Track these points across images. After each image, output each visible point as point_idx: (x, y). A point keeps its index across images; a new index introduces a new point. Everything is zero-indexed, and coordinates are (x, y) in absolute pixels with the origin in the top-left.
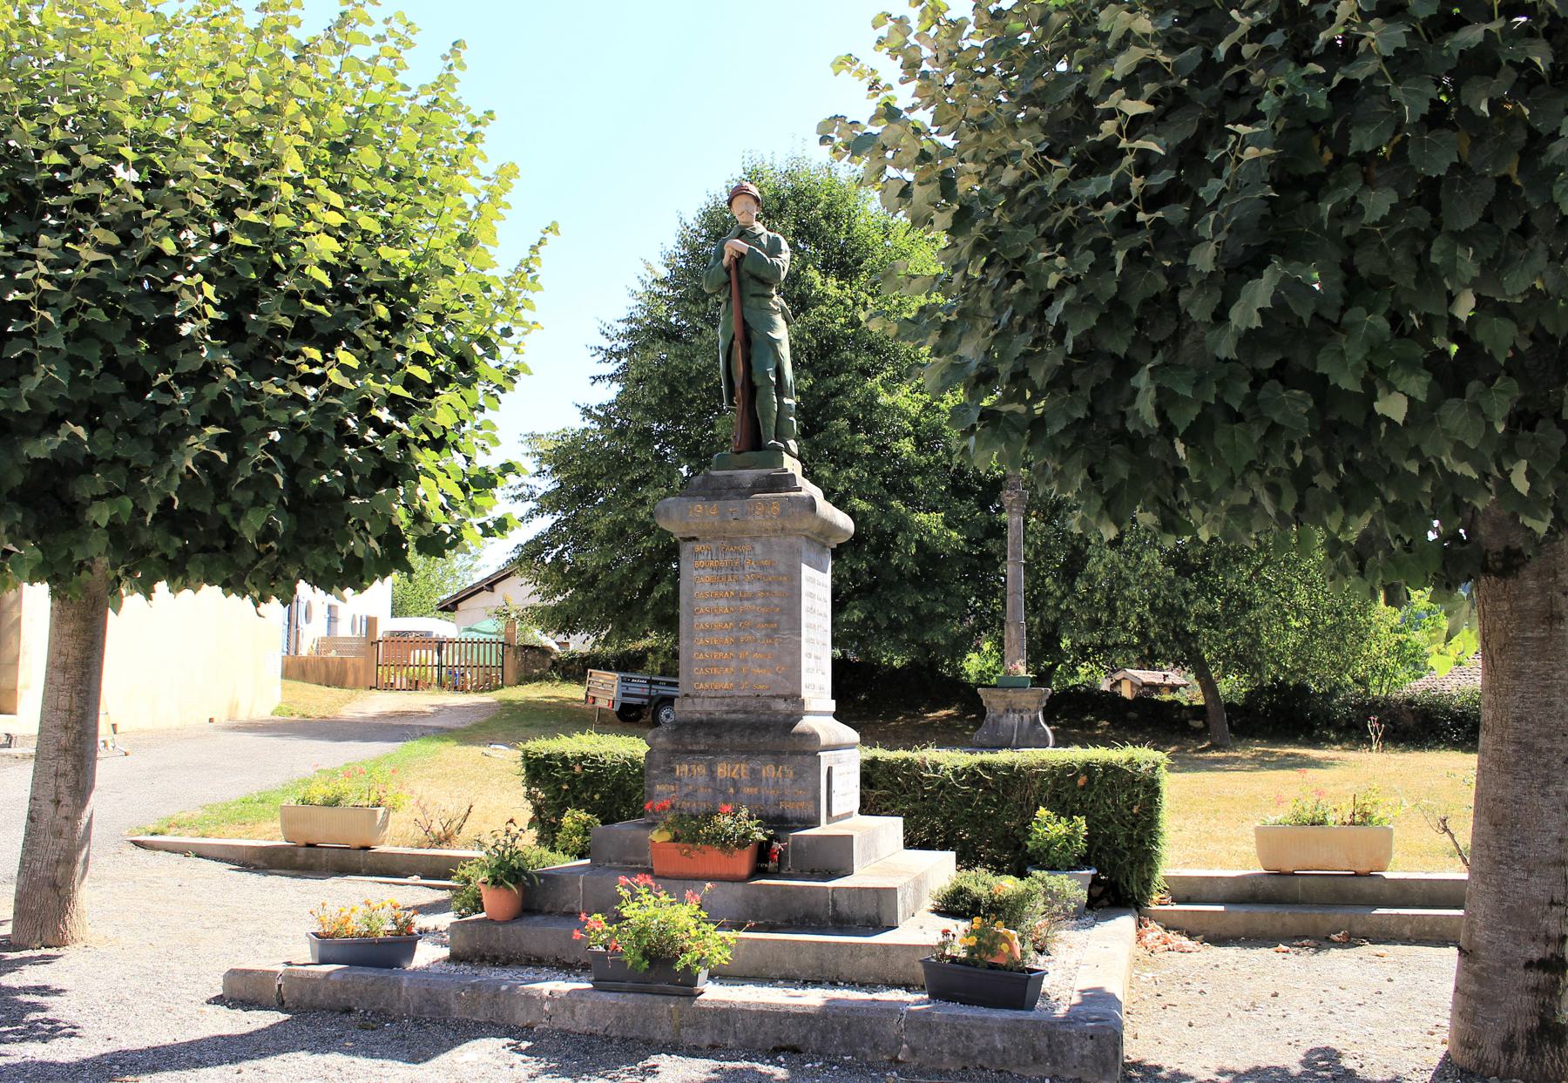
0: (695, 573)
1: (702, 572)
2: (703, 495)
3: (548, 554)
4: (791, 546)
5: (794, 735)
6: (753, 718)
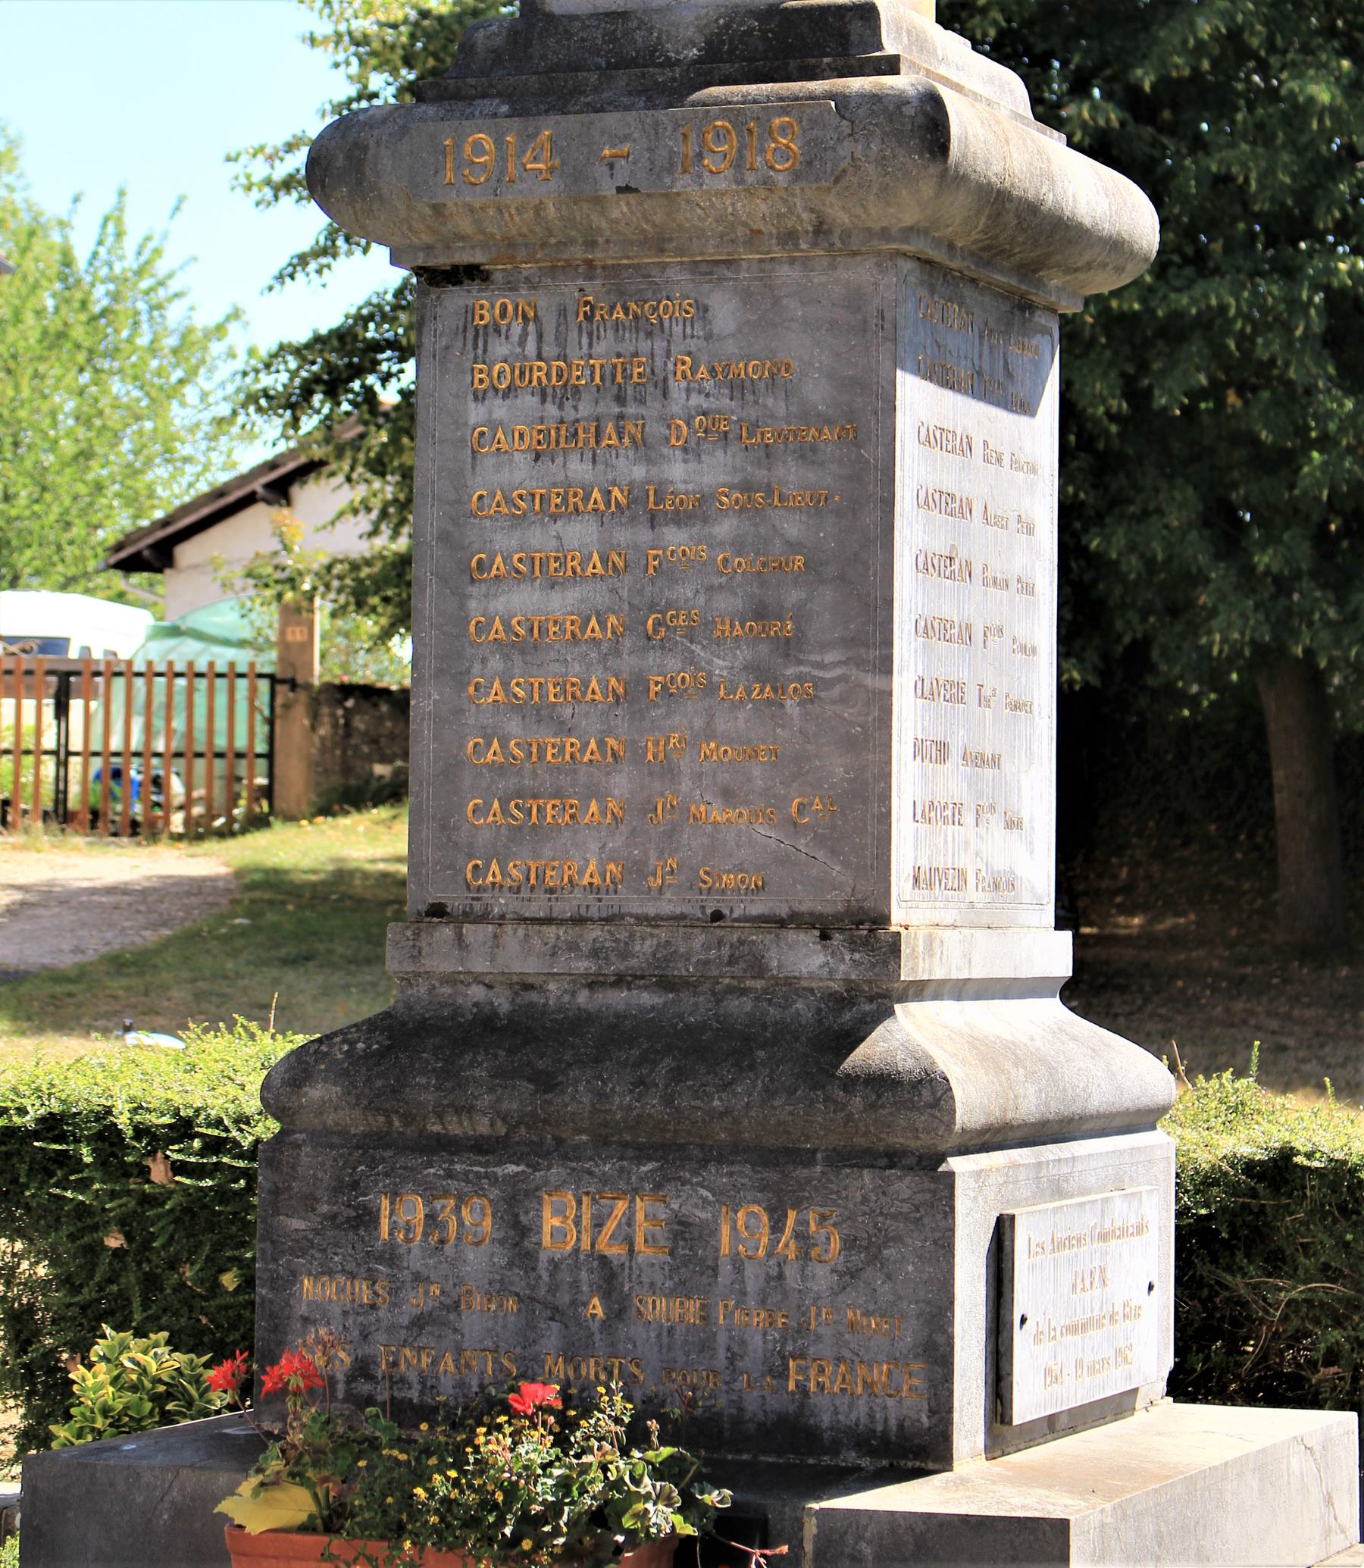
0: (476, 413)
1: (500, 409)
2: (507, 96)
3: (385, 379)
4: (855, 300)
5: (850, 1082)
6: (694, 1008)
